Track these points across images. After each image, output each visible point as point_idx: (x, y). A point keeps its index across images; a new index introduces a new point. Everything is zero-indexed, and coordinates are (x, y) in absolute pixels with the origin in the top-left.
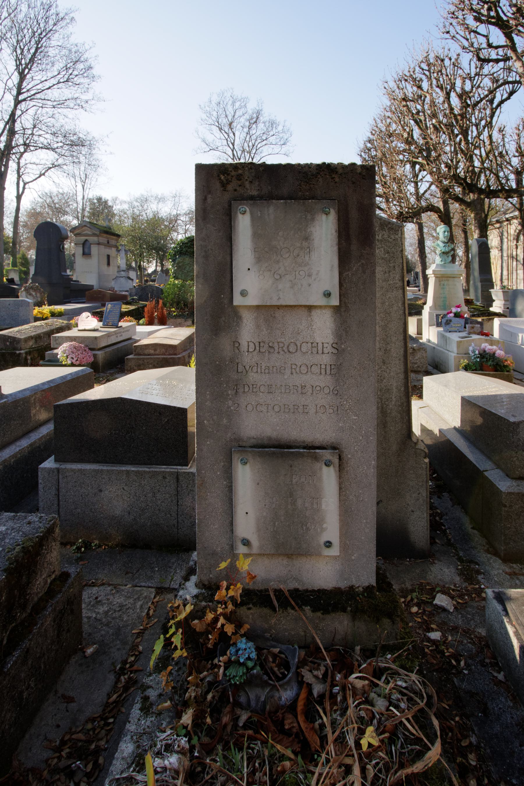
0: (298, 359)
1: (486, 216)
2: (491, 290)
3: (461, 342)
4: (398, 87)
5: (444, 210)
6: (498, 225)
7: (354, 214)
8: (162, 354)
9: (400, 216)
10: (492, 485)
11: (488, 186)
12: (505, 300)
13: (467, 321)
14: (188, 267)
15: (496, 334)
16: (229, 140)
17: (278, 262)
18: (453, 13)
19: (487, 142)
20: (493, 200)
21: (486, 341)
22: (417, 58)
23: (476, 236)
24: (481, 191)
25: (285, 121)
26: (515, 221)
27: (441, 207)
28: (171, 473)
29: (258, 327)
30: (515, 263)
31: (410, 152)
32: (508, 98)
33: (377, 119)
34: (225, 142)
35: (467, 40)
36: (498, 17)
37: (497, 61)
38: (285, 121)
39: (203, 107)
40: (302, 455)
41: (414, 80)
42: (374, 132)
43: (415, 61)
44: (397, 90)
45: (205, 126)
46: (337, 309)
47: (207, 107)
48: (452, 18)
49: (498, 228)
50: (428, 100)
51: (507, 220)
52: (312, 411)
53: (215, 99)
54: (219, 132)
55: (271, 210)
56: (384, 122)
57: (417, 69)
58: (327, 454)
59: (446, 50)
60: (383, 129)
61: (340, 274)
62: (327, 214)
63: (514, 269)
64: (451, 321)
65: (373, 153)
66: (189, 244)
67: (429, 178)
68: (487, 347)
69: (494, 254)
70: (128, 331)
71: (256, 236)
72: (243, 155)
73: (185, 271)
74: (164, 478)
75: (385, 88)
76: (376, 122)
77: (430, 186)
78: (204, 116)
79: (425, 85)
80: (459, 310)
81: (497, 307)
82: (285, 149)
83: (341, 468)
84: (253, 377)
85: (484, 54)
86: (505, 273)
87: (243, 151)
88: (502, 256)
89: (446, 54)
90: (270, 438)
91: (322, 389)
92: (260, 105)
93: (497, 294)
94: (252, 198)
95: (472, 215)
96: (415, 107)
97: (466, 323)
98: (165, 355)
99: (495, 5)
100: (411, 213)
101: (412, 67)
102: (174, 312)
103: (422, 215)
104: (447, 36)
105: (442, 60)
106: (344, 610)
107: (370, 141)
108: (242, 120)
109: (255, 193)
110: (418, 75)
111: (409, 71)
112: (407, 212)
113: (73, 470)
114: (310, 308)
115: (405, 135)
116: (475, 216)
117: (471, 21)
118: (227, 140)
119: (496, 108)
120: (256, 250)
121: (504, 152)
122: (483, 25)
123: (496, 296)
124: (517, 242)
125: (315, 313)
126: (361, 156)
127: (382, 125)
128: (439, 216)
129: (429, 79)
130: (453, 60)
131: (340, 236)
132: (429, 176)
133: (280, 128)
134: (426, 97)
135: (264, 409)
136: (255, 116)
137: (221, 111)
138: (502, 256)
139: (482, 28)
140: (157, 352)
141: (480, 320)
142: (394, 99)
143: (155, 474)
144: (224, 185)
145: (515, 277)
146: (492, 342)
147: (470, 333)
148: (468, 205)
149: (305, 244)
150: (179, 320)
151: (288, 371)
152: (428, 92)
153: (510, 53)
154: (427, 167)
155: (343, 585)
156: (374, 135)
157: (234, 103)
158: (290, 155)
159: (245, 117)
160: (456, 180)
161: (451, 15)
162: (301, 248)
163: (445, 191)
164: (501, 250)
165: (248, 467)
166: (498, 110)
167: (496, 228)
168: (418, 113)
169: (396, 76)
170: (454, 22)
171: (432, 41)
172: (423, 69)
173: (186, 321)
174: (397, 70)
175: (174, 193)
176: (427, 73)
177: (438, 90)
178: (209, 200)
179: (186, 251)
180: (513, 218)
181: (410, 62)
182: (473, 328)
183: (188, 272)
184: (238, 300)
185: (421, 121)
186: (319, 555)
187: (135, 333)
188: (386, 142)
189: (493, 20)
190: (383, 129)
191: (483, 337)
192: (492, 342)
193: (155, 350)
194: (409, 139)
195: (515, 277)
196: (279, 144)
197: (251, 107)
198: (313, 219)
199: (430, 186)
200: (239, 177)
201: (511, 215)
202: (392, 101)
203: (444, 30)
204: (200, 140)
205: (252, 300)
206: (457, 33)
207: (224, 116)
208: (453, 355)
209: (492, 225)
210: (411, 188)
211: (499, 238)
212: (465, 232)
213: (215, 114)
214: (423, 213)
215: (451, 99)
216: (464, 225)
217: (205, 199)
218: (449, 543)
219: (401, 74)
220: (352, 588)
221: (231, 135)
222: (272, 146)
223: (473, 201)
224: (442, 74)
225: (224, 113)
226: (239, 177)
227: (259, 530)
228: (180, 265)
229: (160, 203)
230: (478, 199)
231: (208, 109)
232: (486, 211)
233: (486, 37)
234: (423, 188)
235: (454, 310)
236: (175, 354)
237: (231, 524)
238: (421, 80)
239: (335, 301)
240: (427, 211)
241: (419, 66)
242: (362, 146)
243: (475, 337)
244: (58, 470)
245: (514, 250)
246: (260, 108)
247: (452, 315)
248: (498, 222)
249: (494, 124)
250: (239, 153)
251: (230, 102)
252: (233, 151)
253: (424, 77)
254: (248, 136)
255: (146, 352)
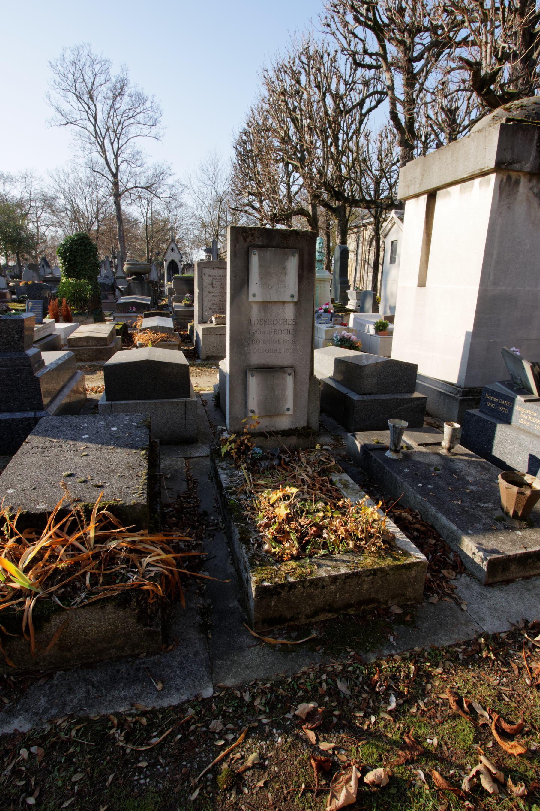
0: (278, 327)
1: (347, 221)
2: (348, 291)
3: (328, 330)
4: (277, 77)
5: (313, 213)
6: (355, 230)
7: (306, 257)
8: (95, 346)
9: (274, 218)
10: (350, 398)
11: (353, 196)
12: (358, 300)
13: (332, 315)
14: (80, 266)
15: (351, 325)
16: (89, 112)
17: (270, 280)
18: (335, 7)
19: (355, 149)
20: (354, 209)
21: (345, 330)
22: (298, 48)
23: (338, 241)
24: (346, 200)
25: (153, 96)
26: (370, 227)
27: (310, 211)
28: (182, 402)
29: (260, 312)
30: (366, 266)
31: (286, 151)
32: (376, 107)
33: (254, 110)
34: (85, 115)
35: (346, 38)
36: (375, 21)
37: (370, 67)
38: (153, 96)
39: (55, 65)
40: (279, 371)
41: (294, 72)
42: (250, 124)
43: (295, 51)
44: (276, 81)
45: (59, 90)
46: (296, 303)
47: (59, 66)
48: (334, 11)
49: (356, 233)
50: (305, 96)
51: (364, 225)
52: (283, 351)
53: (70, 56)
54: (76, 100)
55: (268, 253)
56: (261, 114)
57: (297, 61)
58: (289, 370)
59: (326, 45)
60: (260, 122)
61: (299, 286)
62: (294, 256)
63: (366, 272)
64: (321, 315)
65: (249, 147)
66: (79, 242)
67: (301, 181)
68: (345, 333)
69: (352, 256)
70: (50, 327)
71: (261, 266)
72: (107, 134)
73: (78, 270)
74: (178, 405)
75: (265, 77)
76: (253, 114)
77: (300, 189)
78: (58, 80)
79: (303, 79)
80: (328, 307)
81: (351, 305)
82: (154, 130)
83: (295, 377)
84: (257, 336)
85: (359, 58)
86: (358, 275)
87: (108, 129)
88: (357, 260)
89: (325, 49)
90: (264, 365)
91: (288, 341)
92: (125, 73)
93: (352, 295)
94: (259, 246)
95: (337, 221)
96: (292, 103)
97: (332, 317)
98: (97, 346)
99: (372, 7)
100: (283, 215)
101: (292, 57)
102: (74, 310)
103: (293, 217)
104: (328, 30)
105: (322, 57)
106: (295, 435)
107: (246, 133)
108: (104, 88)
109: (260, 244)
110: (297, 67)
111: (289, 62)
112: (280, 215)
113: (121, 404)
114: (284, 303)
115: (282, 133)
116: (338, 222)
117: (350, 17)
118: (87, 112)
119: (365, 115)
120: (260, 273)
121: (367, 158)
122: (361, 27)
123: (351, 295)
124: (370, 247)
125: (286, 305)
126: (236, 148)
127: (259, 117)
128: (308, 220)
129: (308, 74)
130: (331, 56)
131: (299, 268)
132: (301, 178)
133: (148, 104)
134: (303, 93)
135: (262, 351)
136: (119, 86)
137: (77, 75)
138: (357, 260)
139: (360, 31)
140: (90, 344)
141: (340, 314)
142: (273, 91)
143: (172, 403)
144: (245, 239)
145: (365, 279)
146: (349, 330)
147: (334, 324)
148: (334, 210)
149: (283, 271)
150: (81, 318)
151: (273, 333)
152: (306, 89)
153: (382, 62)
154: (301, 170)
155: (293, 427)
156: (250, 127)
157: (93, 63)
158: (161, 138)
159: (107, 85)
160: (326, 187)
161: (333, 8)
162: (282, 273)
163: (316, 197)
164: (357, 254)
165: (254, 378)
166: (366, 118)
167: (354, 233)
168: (295, 108)
169: (275, 65)
170: (335, 15)
171: (313, 31)
172: (303, 63)
173: (87, 319)
174: (278, 58)
175: (24, 172)
176: (306, 67)
177: (316, 90)
178: (238, 246)
179: (77, 249)
180: (369, 224)
181: (291, 52)
182: (336, 320)
183: (80, 270)
184: (251, 299)
185: (297, 119)
186: (284, 415)
187: (55, 329)
188: (262, 137)
189: (370, 23)
190: (260, 122)
191: (343, 327)
192: (349, 330)
193: (88, 342)
194: (286, 138)
195: (365, 279)
196: (148, 124)
197: (115, 73)
198: (287, 259)
199: (300, 189)
200: (252, 235)
201: (368, 221)
202: (271, 93)
203: (325, 22)
204: (53, 110)
205: (258, 299)
206: (337, 29)
207: (82, 80)
208: (322, 340)
209: (351, 229)
210: (283, 189)
211: (356, 243)
212: (328, 235)
213: (71, 77)
214: (295, 215)
215: (326, 100)
216: (328, 228)
217: (235, 246)
218: (327, 431)
219: (281, 63)
220: (296, 428)
221: (92, 107)
222: (139, 125)
223: (339, 207)
224: (320, 73)
225: (81, 77)
226: (252, 235)
227: (258, 405)
228: (72, 263)
229: (7, 184)
230: (342, 205)
231: (60, 68)
232: (347, 215)
233: (363, 41)
234: (294, 189)
235: (324, 307)
236: (107, 345)
237: (246, 404)
238: (300, 73)
239: (296, 300)
240: (298, 215)
241: (300, 59)
242: (237, 138)
243: (338, 327)
244: (111, 405)
245: (367, 254)
246: (125, 77)
247: (322, 311)
248: (356, 227)
249: (361, 131)
250: (103, 131)
251: (88, 64)
252: (95, 126)
253: (302, 71)
254: (113, 110)
255: (80, 344)
